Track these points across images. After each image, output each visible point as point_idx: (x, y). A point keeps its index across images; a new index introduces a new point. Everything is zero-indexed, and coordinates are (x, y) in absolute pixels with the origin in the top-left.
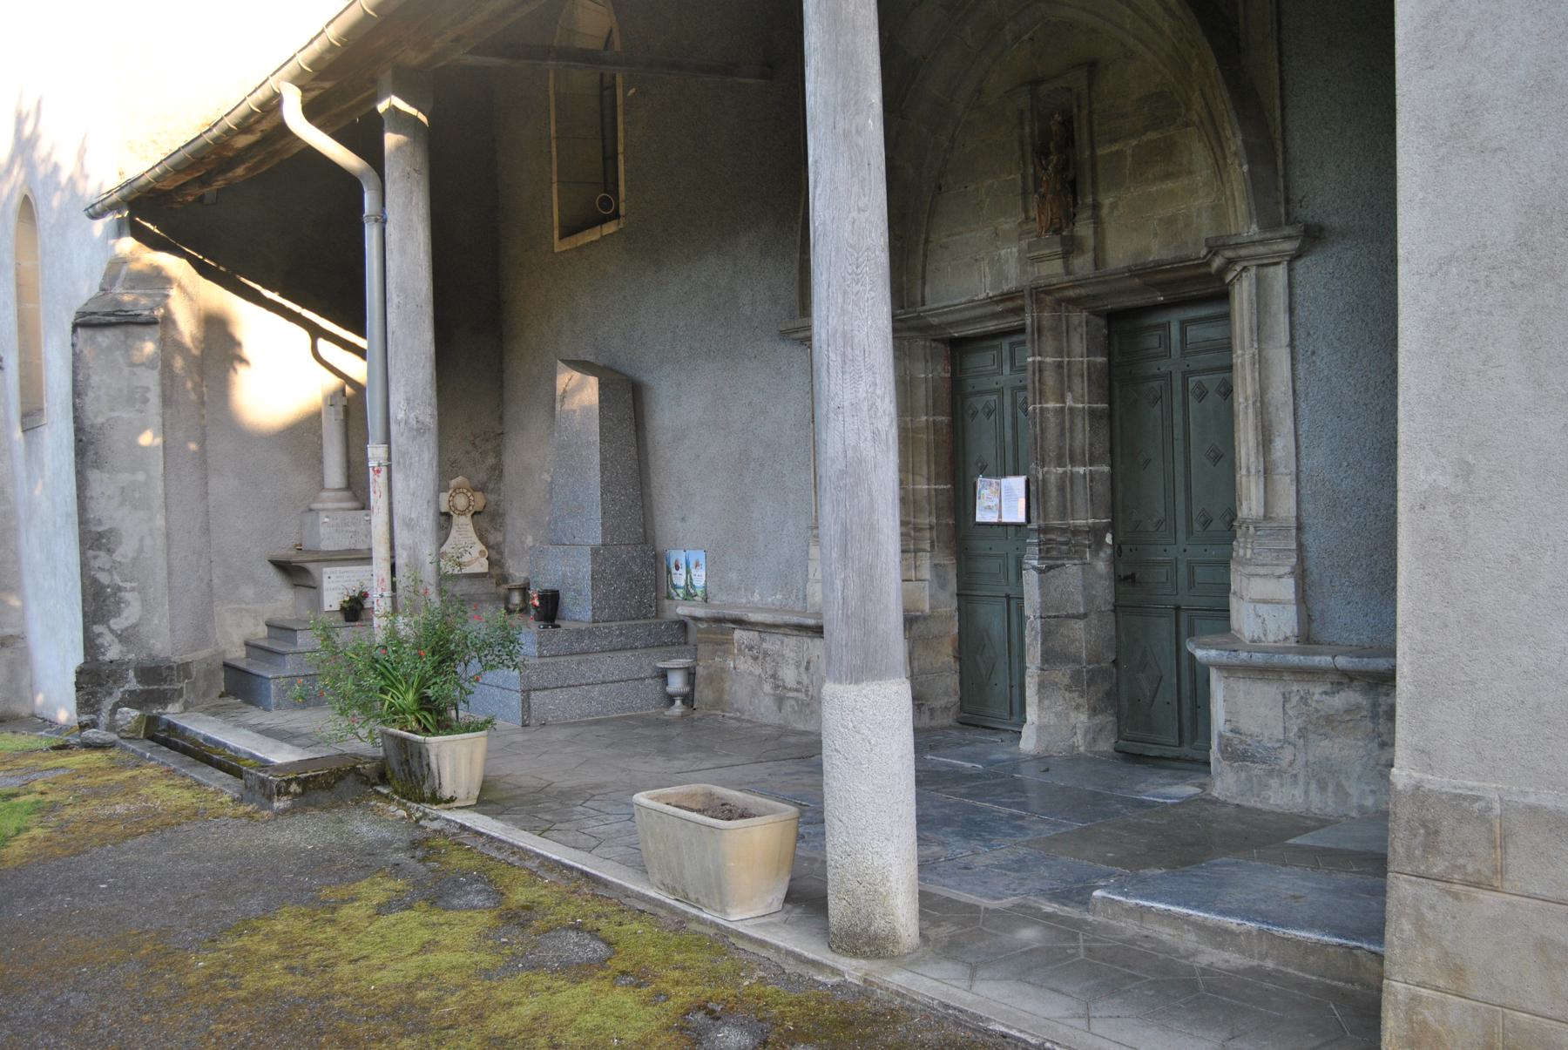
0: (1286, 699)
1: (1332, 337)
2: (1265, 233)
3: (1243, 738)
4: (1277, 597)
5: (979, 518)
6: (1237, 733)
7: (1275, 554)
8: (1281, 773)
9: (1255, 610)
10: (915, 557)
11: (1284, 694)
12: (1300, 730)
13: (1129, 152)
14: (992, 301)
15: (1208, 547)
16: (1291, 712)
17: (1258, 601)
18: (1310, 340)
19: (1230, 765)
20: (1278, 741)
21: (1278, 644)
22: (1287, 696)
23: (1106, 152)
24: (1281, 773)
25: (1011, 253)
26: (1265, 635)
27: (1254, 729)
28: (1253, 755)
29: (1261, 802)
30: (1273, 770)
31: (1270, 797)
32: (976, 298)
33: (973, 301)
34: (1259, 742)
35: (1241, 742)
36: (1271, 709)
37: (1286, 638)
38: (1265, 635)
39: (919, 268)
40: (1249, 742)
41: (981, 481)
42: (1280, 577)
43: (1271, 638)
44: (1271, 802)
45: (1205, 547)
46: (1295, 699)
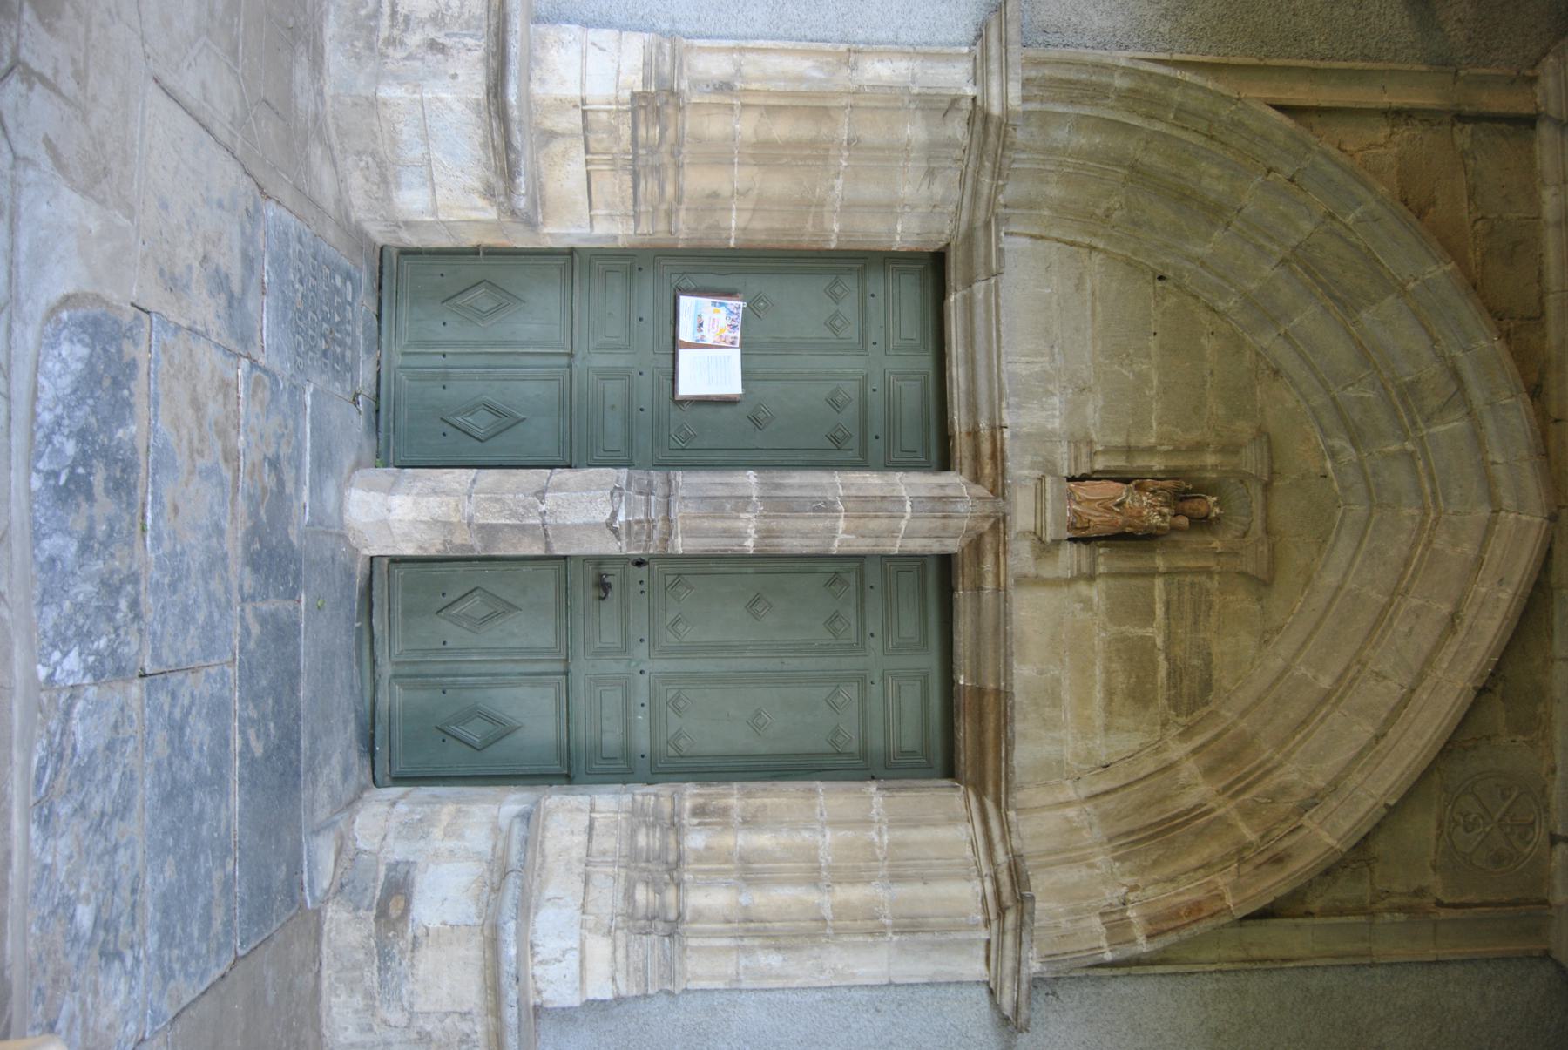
0: (464, 1015)
1: (894, 1034)
2: (1028, 982)
3: (408, 955)
4: (589, 977)
5: (686, 302)
6: (414, 945)
7: (641, 966)
8: (371, 1009)
9: (572, 949)
10: (626, 215)
11: (469, 1013)
12: (429, 1034)
13: (1149, 632)
14: (996, 428)
15: (646, 708)
16: (448, 1021)
17: (582, 951)
18: (894, 1006)
19: (370, 936)
20: (411, 1004)
21: (531, 982)
22: (468, 1017)
23: (1157, 593)
24: (371, 1009)
25: (1054, 416)
26: (541, 962)
27: (422, 969)
28: (388, 968)
29: (331, 984)
30: (373, 998)
31: (338, 996)
32: (1004, 404)
33: (1001, 399)
34: (406, 977)
35: (402, 952)
36: (449, 994)
37: (539, 992)
38: (541, 962)
39: (1054, 233)
40: (404, 963)
41: (736, 305)
42: (614, 979)
43: (538, 971)
44: (333, 1000)
45: (647, 704)
46: (465, 1027)
